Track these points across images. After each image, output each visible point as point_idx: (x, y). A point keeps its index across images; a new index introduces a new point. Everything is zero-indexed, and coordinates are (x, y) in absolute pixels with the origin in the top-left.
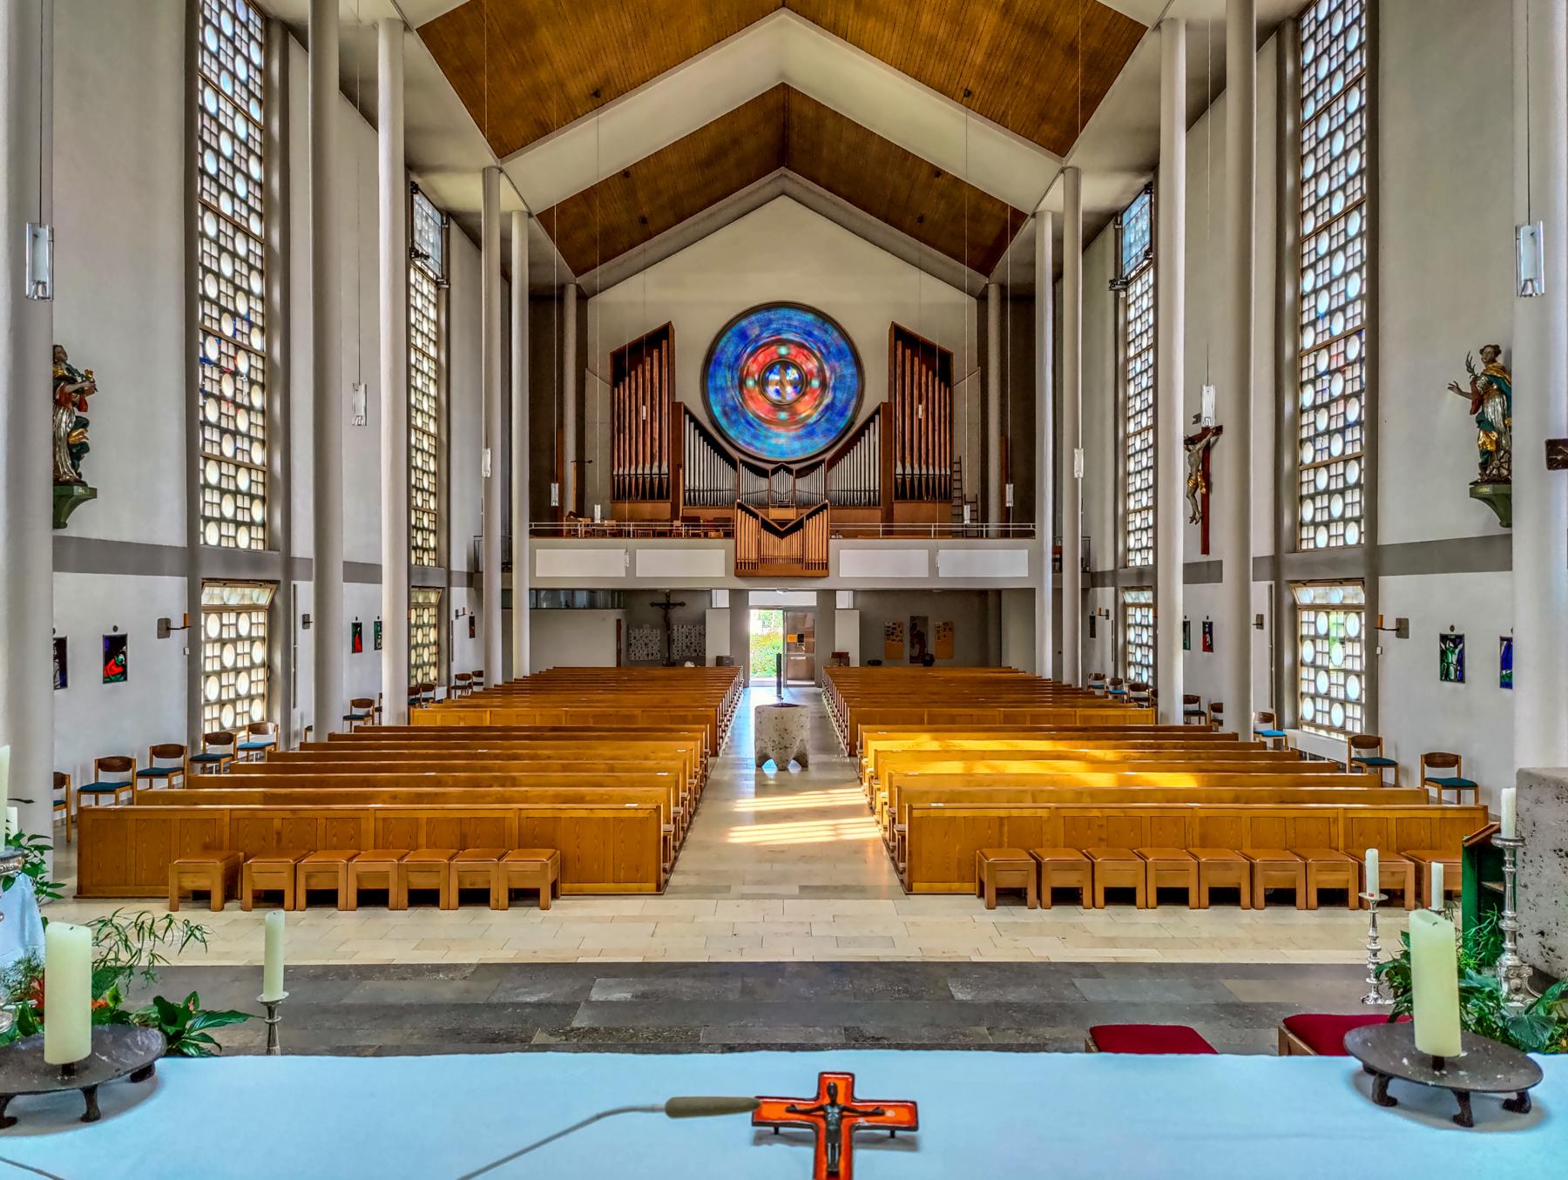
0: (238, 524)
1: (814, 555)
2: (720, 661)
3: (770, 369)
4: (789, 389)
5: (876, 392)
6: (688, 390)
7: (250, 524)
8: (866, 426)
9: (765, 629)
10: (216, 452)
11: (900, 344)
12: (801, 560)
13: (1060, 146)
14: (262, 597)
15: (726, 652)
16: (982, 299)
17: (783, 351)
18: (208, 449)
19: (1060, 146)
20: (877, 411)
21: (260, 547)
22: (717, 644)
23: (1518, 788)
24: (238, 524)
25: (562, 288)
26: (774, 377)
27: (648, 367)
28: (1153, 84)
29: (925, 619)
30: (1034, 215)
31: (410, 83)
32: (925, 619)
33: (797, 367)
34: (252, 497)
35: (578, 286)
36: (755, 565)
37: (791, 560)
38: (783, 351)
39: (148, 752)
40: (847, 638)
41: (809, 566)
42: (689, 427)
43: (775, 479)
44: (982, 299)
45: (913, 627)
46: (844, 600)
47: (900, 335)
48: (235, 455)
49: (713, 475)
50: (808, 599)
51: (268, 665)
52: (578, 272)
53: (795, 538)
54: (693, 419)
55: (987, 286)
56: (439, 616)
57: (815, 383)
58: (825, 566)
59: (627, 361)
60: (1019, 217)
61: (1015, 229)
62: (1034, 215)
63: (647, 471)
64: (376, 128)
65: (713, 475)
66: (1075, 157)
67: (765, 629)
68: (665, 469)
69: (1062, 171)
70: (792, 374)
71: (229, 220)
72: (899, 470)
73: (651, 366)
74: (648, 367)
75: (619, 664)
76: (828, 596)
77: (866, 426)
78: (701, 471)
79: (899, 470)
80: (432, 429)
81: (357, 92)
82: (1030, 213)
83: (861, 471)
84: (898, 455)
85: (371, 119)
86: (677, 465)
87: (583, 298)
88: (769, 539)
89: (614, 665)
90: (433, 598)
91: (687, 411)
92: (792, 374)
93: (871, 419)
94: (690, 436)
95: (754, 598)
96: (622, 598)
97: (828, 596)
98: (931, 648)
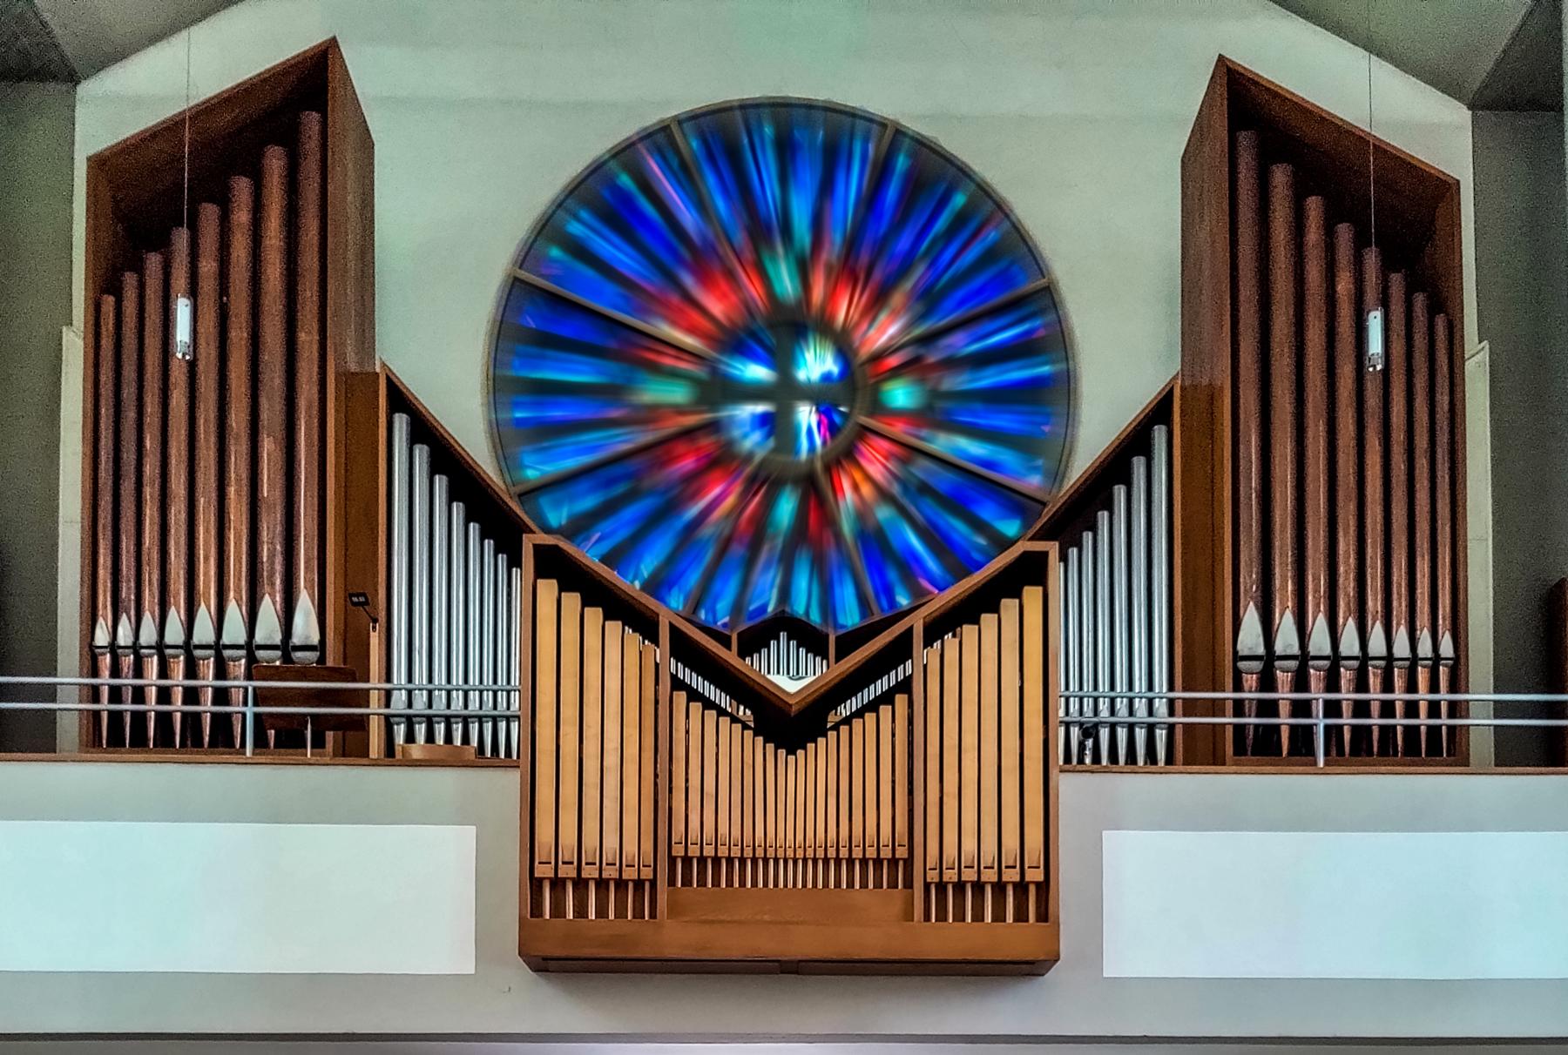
1: (970, 836)
4: (806, 416)
12: (895, 868)
20: (1160, 411)
27: (242, 216)
36: (634, 891)
37: (846, 863)
41: (952, 894)
42: (406, 464)
47: (1253, 126)
53: (867, 743)
54: (424, 430)
58: (1035, 896)
68: (305, 626)
70: (816, 363)
72: (1250, 637)
73: (255, 210)
74: (242, 216)
79: (1250, 637)
84: (1250, 579)
86: (359, 606)
88: (719, 745)
91: (399, 399)
92: (816, 363)
93: (1136, 442)
94: (413, 498)
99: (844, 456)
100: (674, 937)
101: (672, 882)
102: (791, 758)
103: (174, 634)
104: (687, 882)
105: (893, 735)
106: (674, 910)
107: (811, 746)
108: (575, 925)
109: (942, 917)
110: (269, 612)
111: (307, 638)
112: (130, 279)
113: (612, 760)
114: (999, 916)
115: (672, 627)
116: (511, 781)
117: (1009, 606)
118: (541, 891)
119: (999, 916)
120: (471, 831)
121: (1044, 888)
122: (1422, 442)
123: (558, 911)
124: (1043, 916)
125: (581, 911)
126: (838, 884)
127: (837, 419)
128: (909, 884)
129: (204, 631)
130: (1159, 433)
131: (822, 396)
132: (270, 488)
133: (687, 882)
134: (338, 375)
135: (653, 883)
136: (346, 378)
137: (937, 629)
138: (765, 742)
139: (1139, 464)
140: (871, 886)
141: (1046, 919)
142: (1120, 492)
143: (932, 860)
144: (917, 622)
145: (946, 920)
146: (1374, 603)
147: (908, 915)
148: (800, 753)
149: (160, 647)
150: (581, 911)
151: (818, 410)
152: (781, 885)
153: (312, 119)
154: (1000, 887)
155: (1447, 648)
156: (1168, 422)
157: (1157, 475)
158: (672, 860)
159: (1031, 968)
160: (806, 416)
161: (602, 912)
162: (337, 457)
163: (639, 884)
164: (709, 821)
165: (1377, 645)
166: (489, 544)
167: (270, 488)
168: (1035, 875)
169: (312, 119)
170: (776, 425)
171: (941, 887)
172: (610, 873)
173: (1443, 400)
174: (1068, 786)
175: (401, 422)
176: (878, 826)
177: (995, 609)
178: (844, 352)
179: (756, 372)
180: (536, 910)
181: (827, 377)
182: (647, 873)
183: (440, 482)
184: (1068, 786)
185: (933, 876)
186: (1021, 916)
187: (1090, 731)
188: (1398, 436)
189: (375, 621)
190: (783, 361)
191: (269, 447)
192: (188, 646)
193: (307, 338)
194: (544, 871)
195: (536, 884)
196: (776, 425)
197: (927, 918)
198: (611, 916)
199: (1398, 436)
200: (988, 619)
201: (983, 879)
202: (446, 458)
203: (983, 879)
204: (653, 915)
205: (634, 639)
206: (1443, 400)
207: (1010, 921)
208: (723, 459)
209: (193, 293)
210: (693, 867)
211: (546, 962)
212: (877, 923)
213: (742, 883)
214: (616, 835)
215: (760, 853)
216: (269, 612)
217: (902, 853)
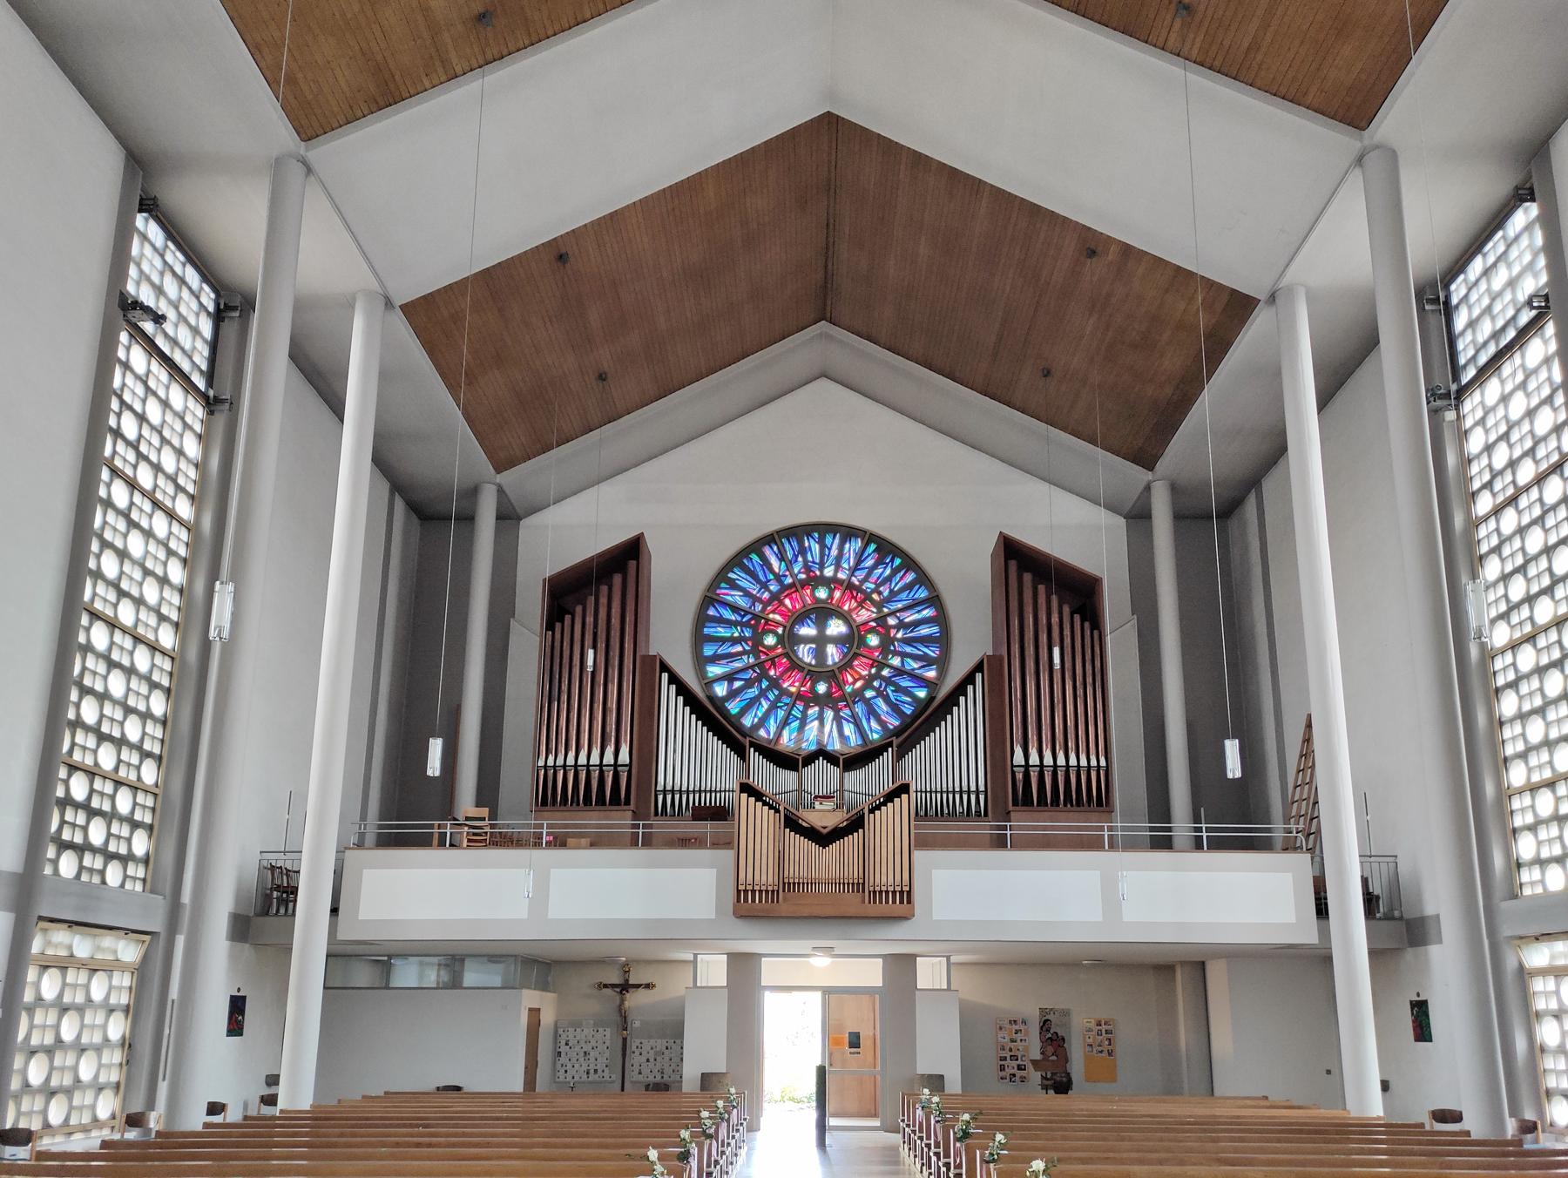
0: (110, 857)
1: (884, 877)
2: (708, 1081)
3: (801, 618)
5: (973, 638)
6: (668, 637)
7: (125, 860)
8: (960, 689)
9: (792, 1038)
10: (133, 777)
11: (1013, 564)
12: (859, 886)
13: (1355, 108)
14: (129, 952)
15: (720, 1066)
16: (1139, 517)
17: (822, 593)
18: (77, 756)
19: (1355, 108)
20: (979, 667)
21: (139, 887)
22: (703, 1051)
23: (1390, 1128)
24: (110, 857)
25: (472, 493)
26: (808, 631)
27: (603, 601)
28: (1273, 377)
29: (1066, 1013)
30: (1272, 298)
31: (387, 377)
32: (1066, 1013)
33: (845, 618)
34: (135, 825)
35: (501, 491)
36: (772, 895)
38: (822, 593)
39: (258, 1100)
40: (939, 1049)
41: (875, 895)
42: (668, 692)
43: (808, 771)
44: (1139, 517)
45: (1045, 1025)
46: (930, 974)
47: (1012, 553)
48: (116, 769)
49: (703, 763)
50: (870, 974)
51: (128, 1045)
52: (502, 464)
54: (674, 679)
55: (1148, 488)
56: (139, 989)
57: (873, 640)
58: (906, 896)
59: (569, 593)
60: (1239, 307)
61: (1219, 345)
62: (1272, 298)
63: (595, 760)
64: (342, 421)
65: (703, 763)
66: (1391, 122)
67: (792, 1038)
68: (624, 757)
69: (1360, 161)
71: (149, 495)
72: (1019, 758)
74: (603, 601)
75: (530, 1082)
76: (901, 966)
77: (960, 689)
78: (688, 758)
79: (1019, 758)
80: (167, 638)
81: (321, 379)
82: (1261, 295)
83: (954, 756)
84: (1017, 733)
85: (338, 411)
87: (509, 517)
89: (518, 1086)
90: (129, 952)
91: (664, 667)
92: (836, 628)
93: (969, 679)
94: (671, 705)
95: (770, 971)
96: (539, 965)
97: (901, 966)
98: (1077, 1068)
99: (846, 665)
103: (571, 761)
110: (610, 750)
112: (558, 625)
114: (894, 902)
116: (731, 854)
117: (897, 800)
119: (894, 902)
121: (909, 892)
122: (1089, 680)
124: (909, 902)
125: (753, 900)
129: (582, 760)
130: (979, 677)
131: (837, 640)
136: (645, 658)
137: (872, 811)
139: (970, 688)
142: (962, 699)
146: (1071, 744)
149: (565, 766)
150: (753, 900)
153: (632, 564)
154: (894, 892)
155: (1103, 763)
157: (976, 691)
164: (793, 872)
165: (1073, 761)
166: (688, 709)
169: (632, 564)
170: (820, 654)
173: (1098, 664)
174: (917, 854)
175: (665, 676)
176: (854, 873)
183: (681, 699)
184: (917, 854)
186: (902, 902)
192: (576, 765)
193: (628, 645)
196: (820, 654)
202: (682, 689)
206: (1098, 664)
208: (795, 665)
209: (595, 647)
210: (789, 886)
216: (610, 750)
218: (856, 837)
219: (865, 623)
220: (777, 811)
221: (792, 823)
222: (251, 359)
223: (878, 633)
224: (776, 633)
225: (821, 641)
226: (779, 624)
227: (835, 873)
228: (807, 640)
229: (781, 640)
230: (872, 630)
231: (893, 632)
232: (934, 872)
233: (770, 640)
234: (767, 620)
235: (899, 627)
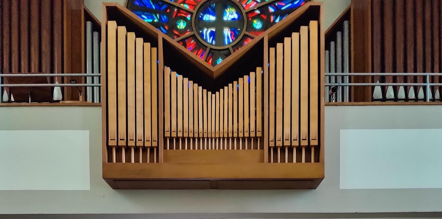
1: (289, 128)
4: (227, 32)
12: (256, 141)
20: (346, 16)
41: (279, 151)
58: (313, 152)
88: (183, 88)
92: (230, 15)
100: (165, 170)
101: (165, 148)
102: (214, 95)
104: (171, 148)
105: (256, 92)
106: (166, 159)
107: (221, 90)
108: (127, 167)
109: (276, 160)
111: (58, 98)
113: (140, 96)
115: (164, 40)
118: (113, 151)
120: (87, 132)
121: (318, 148)
123: (119, 159)
124: (317, 160)
126: (233, 148)
127: (237, 33)
128: (262, 147)
130: (346, 23)
131: (232, 25)
132: (46, 48)
133: (171, 148)
134: (67, 10)
135: (158, 148)
137: (273, 43)
138: (203, 89)
139: (339, 34)
140: (246, 148)
141: (318, 161)
143: (272, 137)
144: (266, 36)
145: (277, 162)
147: (262, 160)
148: (217, 93)
150: (128, 160)
151: (231, 31)
152: (210, 148)
154: (299, 149)
156: (349, 19)
158: (165, 139)
159: (310, 184)
160: (227, 32)
161: (137, 160)
162: (68, 40)
163: (152, 149)
164: (181, 122)
167: (46, 48)
168: (314, 143)
171: (275, 149)
172: (139, 144)
175: (89, 24)
176: (249, 124)
177: (298, 30)
178: (239, 12)
179: (209, 18)
180: (110, 159)
181: (234, 19)
182: (155, 144)
185: (272, 144)
187: (335, 90)
188: (428, 24)
189: (81, 92)
190: (220, 16)
191: (45, 35)
194: (111, 143)
195: (109, 149)
197: (270, 161)
198: (141, 161)
199: (428, 24)
200: (295, 35)
201: (293, 144)
203: (293, 144)
204: (157, 161)
205: (148, 45)
207: (301, 164)
210: (174, 141)
211: (118, 184)
212: (249, 164)
213: (194, 148)
214: (142, 131)
215: (201, 135)
217: (259, 134)
218: (248, 83)
219: (253, 11)
220: (154, 44)
221: (174, 60)
222: (33, 68)
223: (262, 20)
224: (185, 19)
225: (220, 23)
226: (188, 12)
227: (226, 127)
228: (209, 24)
229: (189, 25)
230: (257, 17)
231: (272, 18)
232: (341, 130)
233: (182, 25)
234: (179, 9)
235: (276, 14)
